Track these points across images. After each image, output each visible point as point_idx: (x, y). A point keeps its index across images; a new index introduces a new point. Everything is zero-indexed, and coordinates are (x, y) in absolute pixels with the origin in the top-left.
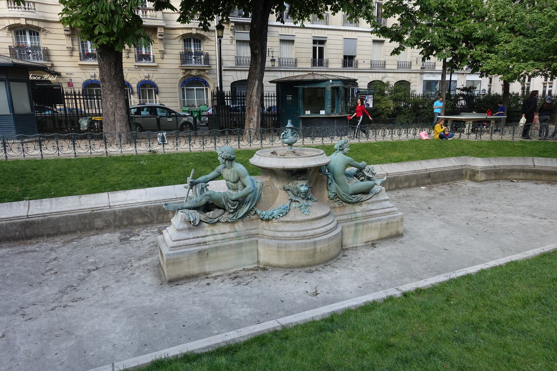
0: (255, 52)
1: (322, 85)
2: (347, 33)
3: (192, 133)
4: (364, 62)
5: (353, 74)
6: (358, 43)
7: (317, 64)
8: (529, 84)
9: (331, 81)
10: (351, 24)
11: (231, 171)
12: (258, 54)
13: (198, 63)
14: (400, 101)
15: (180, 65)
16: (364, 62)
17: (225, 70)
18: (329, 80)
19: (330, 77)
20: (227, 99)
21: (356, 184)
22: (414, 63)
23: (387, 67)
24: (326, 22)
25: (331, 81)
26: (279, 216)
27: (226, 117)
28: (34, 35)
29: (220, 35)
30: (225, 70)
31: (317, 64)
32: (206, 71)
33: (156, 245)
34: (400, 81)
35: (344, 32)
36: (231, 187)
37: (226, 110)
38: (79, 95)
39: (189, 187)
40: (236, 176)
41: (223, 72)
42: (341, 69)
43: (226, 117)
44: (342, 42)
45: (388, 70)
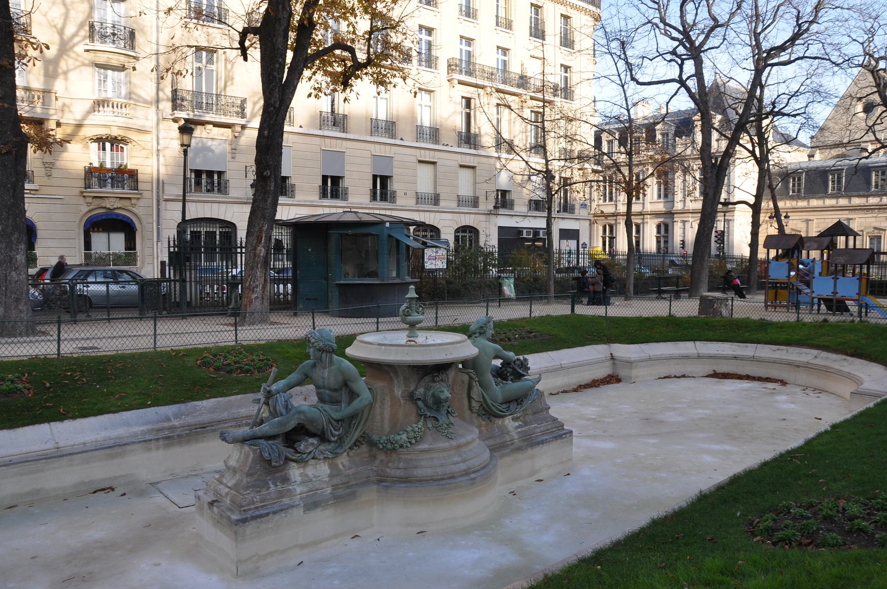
0: (265, 173)
1: (373, 230)
2: (377, 146)
3: (67, 317)
4: (405, 194)
5: (422, 214)
6: (346, 158)
7: (329, 195)
8: (667, 237)
9: (388, 225)
10: (334, 128)
11: (329, 372)
12: (269, 177)
13: (118, 187)
14: (255, 255)
15: (83, 190)
16: (405, 194)
17: (166, 200)
18: (383, 222)
19: (385, 219)
20: (241, 253)
21: (499, 390)
22: (482, 199)
23: (442, 203)
24: (344, 127)
25: (388, 225)
26: (410, 442)
27: (193, 284)
28: (117, 151)
29: (185, 143)
30: (166, 200)
31: (329, 195)
32: (133, 201)
33: (242, 506)
34: (462, 227)
35: (372, 145)
36: (327, 398)
37: (193, 272)
38: (241, 247)
39: (263, 400)
40: (340, 379)
41: (163, 203)
42: (455, 209)
43: (193, 284)
44: (369, 161)
45: (400, 206)
